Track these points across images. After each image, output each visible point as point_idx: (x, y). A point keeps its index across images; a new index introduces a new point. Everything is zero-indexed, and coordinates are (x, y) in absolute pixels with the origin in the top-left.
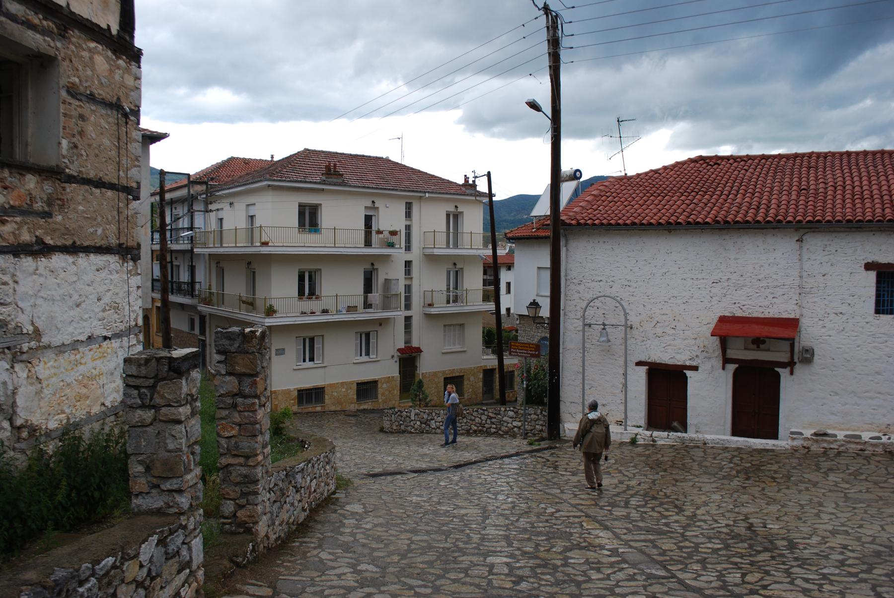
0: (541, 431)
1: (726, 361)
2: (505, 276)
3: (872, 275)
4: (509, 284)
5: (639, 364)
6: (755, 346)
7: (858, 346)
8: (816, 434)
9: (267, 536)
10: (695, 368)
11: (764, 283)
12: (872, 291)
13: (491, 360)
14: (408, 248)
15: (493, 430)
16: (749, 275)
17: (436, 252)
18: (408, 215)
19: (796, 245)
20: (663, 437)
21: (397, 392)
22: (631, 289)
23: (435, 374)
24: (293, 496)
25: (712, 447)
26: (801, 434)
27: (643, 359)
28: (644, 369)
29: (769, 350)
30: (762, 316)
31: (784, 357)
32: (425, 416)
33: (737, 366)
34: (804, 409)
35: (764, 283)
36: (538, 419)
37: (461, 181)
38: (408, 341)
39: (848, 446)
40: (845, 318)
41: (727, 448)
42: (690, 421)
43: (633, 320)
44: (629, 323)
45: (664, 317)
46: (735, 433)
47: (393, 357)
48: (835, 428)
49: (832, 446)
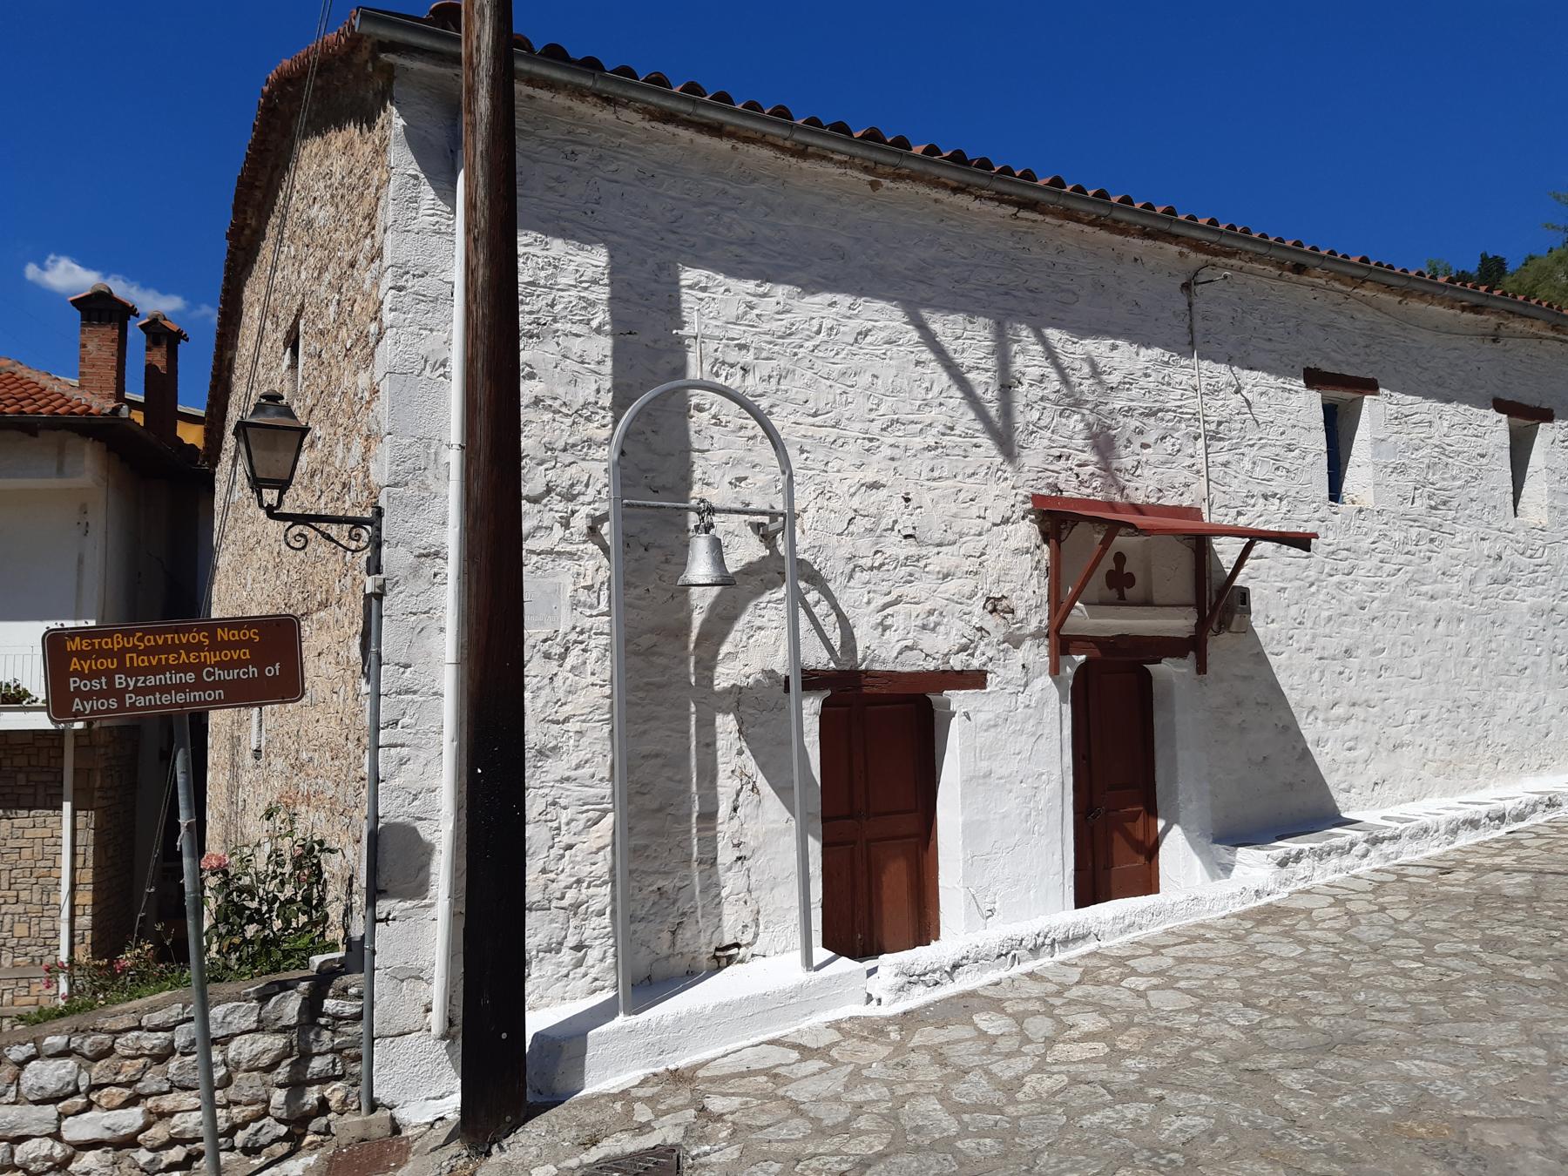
20: (883, 984)
31: (1179, 624)
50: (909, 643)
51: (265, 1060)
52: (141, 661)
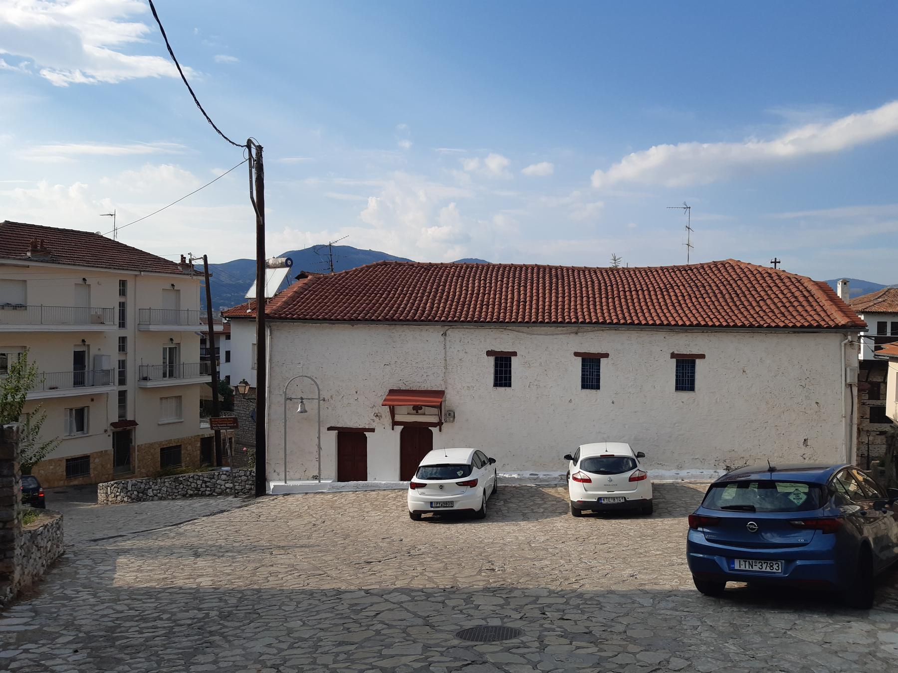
0: (251, 489)
1: (395, 423)
2: (223, 346)
3: (492, 360)
4: (228, 353)
5: (330, 429)
9: (19, 582)
13: (205, 427)
14: (122, 325)
15: (207, 493)
18: (123, 292)
19: (442, 338)
21: (110, 466)
23: (151, 445)
24: (36, 554)
31: (435, 420)
32: (143, 486)
36: (248, 480)
37: (178, 260)
38: (122, 415)
43: (325, 394)
47: (106, 431)
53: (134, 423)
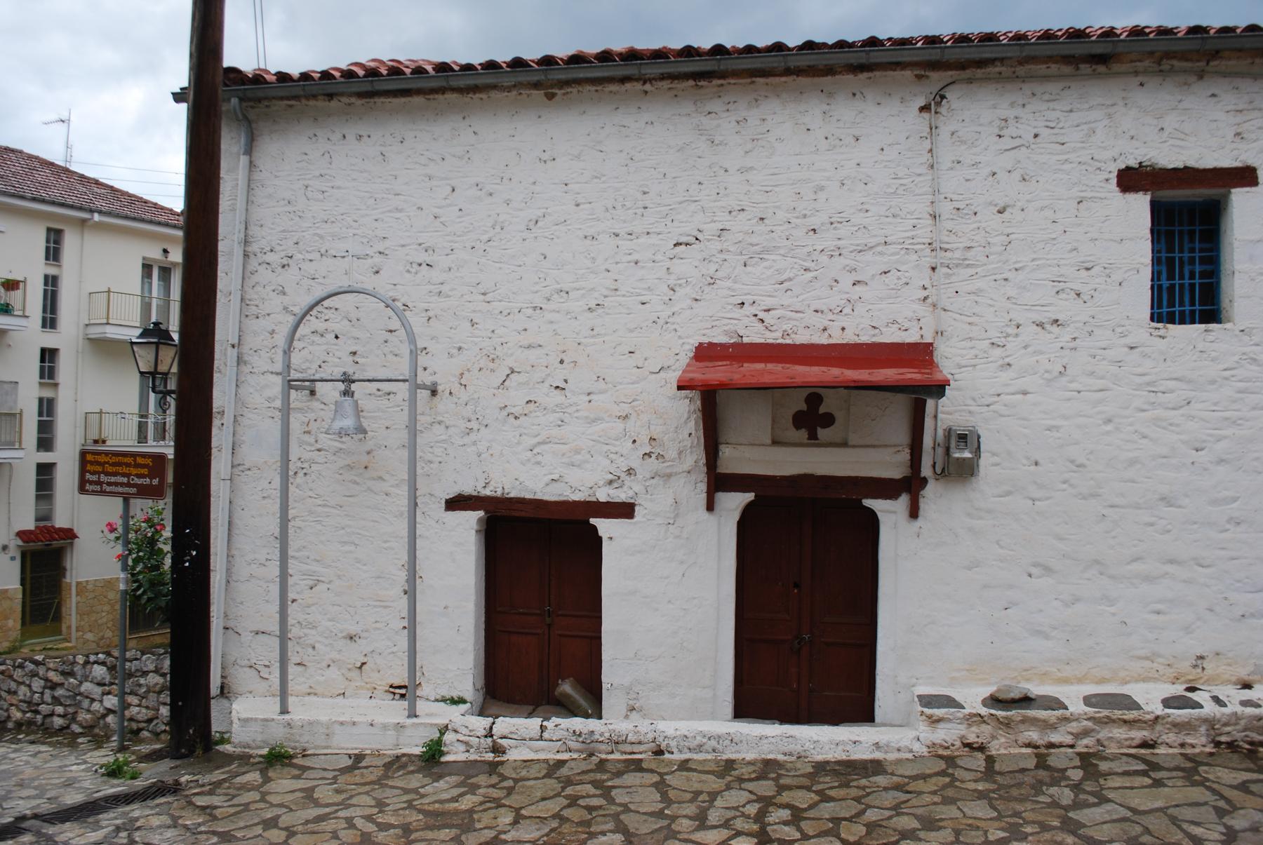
1: (718, 482)
3: (1140, 205)
5: (457, 503)
6: (803, 434)
7: (1109, 421)
8: (995, 701)
10: (625, 510)
11: (827, 240)
12: (1142, 251)
14: (50, 322)
15: (58, 722)
16: (781, 215)
17: (112, 332)
18: (53, 253)
20: (528, 736)
22: (435, 275)
25: (684, 766)
26: (950, 702)
27: (468, 488)
28: (471, 519)
29: (844, 444)
30: (823, 340)
31: (891, 465)
33: (750, 496)
34: (951, 616)
35: (827, 240)
39: (1104, 734)
40: (1065, 335)
41: (730, 764)
42: (610, 675)
43: (439, 368)
44: (424, 378)
45: (532, 355)
46: (745, 708)
48: (1044, 677)
49: (1055, 738)
50: (556, 477)
51: (157, 689)
52: (110, 469)
53: (69, 534)
